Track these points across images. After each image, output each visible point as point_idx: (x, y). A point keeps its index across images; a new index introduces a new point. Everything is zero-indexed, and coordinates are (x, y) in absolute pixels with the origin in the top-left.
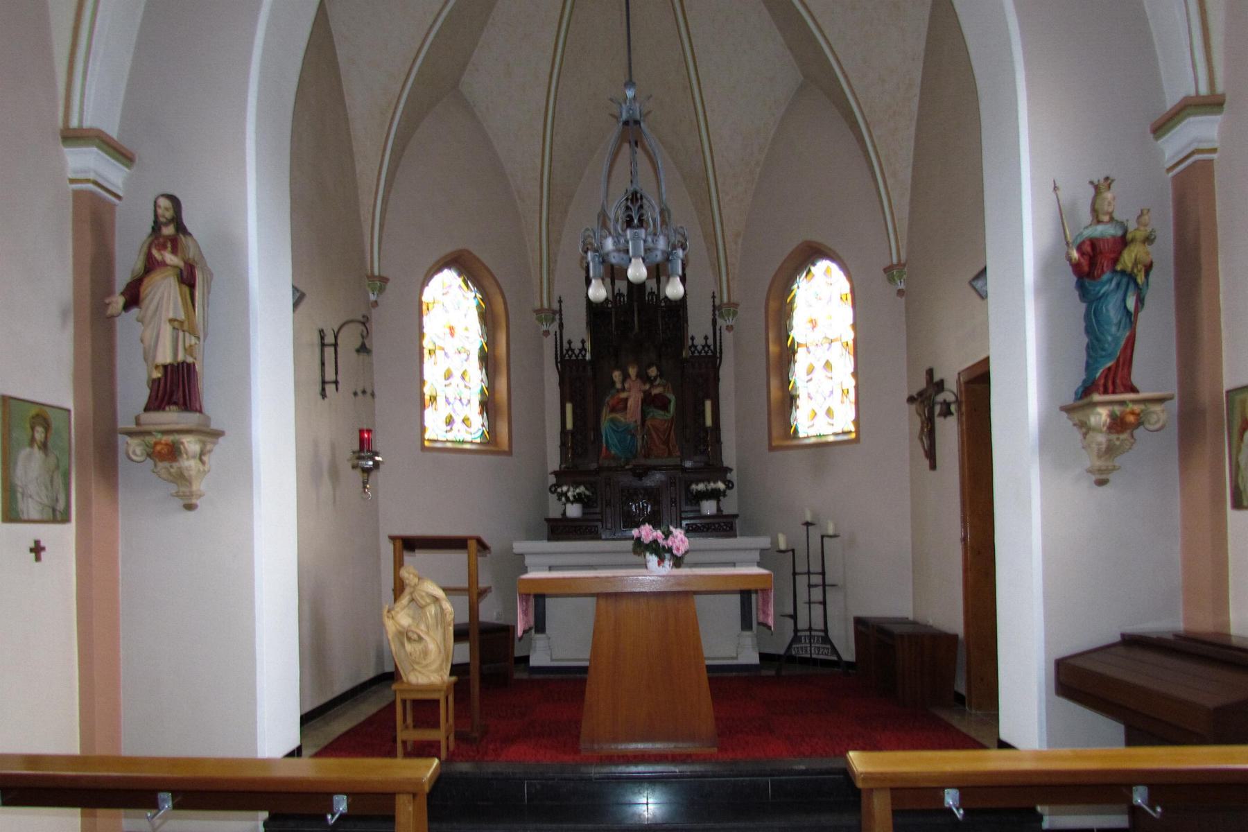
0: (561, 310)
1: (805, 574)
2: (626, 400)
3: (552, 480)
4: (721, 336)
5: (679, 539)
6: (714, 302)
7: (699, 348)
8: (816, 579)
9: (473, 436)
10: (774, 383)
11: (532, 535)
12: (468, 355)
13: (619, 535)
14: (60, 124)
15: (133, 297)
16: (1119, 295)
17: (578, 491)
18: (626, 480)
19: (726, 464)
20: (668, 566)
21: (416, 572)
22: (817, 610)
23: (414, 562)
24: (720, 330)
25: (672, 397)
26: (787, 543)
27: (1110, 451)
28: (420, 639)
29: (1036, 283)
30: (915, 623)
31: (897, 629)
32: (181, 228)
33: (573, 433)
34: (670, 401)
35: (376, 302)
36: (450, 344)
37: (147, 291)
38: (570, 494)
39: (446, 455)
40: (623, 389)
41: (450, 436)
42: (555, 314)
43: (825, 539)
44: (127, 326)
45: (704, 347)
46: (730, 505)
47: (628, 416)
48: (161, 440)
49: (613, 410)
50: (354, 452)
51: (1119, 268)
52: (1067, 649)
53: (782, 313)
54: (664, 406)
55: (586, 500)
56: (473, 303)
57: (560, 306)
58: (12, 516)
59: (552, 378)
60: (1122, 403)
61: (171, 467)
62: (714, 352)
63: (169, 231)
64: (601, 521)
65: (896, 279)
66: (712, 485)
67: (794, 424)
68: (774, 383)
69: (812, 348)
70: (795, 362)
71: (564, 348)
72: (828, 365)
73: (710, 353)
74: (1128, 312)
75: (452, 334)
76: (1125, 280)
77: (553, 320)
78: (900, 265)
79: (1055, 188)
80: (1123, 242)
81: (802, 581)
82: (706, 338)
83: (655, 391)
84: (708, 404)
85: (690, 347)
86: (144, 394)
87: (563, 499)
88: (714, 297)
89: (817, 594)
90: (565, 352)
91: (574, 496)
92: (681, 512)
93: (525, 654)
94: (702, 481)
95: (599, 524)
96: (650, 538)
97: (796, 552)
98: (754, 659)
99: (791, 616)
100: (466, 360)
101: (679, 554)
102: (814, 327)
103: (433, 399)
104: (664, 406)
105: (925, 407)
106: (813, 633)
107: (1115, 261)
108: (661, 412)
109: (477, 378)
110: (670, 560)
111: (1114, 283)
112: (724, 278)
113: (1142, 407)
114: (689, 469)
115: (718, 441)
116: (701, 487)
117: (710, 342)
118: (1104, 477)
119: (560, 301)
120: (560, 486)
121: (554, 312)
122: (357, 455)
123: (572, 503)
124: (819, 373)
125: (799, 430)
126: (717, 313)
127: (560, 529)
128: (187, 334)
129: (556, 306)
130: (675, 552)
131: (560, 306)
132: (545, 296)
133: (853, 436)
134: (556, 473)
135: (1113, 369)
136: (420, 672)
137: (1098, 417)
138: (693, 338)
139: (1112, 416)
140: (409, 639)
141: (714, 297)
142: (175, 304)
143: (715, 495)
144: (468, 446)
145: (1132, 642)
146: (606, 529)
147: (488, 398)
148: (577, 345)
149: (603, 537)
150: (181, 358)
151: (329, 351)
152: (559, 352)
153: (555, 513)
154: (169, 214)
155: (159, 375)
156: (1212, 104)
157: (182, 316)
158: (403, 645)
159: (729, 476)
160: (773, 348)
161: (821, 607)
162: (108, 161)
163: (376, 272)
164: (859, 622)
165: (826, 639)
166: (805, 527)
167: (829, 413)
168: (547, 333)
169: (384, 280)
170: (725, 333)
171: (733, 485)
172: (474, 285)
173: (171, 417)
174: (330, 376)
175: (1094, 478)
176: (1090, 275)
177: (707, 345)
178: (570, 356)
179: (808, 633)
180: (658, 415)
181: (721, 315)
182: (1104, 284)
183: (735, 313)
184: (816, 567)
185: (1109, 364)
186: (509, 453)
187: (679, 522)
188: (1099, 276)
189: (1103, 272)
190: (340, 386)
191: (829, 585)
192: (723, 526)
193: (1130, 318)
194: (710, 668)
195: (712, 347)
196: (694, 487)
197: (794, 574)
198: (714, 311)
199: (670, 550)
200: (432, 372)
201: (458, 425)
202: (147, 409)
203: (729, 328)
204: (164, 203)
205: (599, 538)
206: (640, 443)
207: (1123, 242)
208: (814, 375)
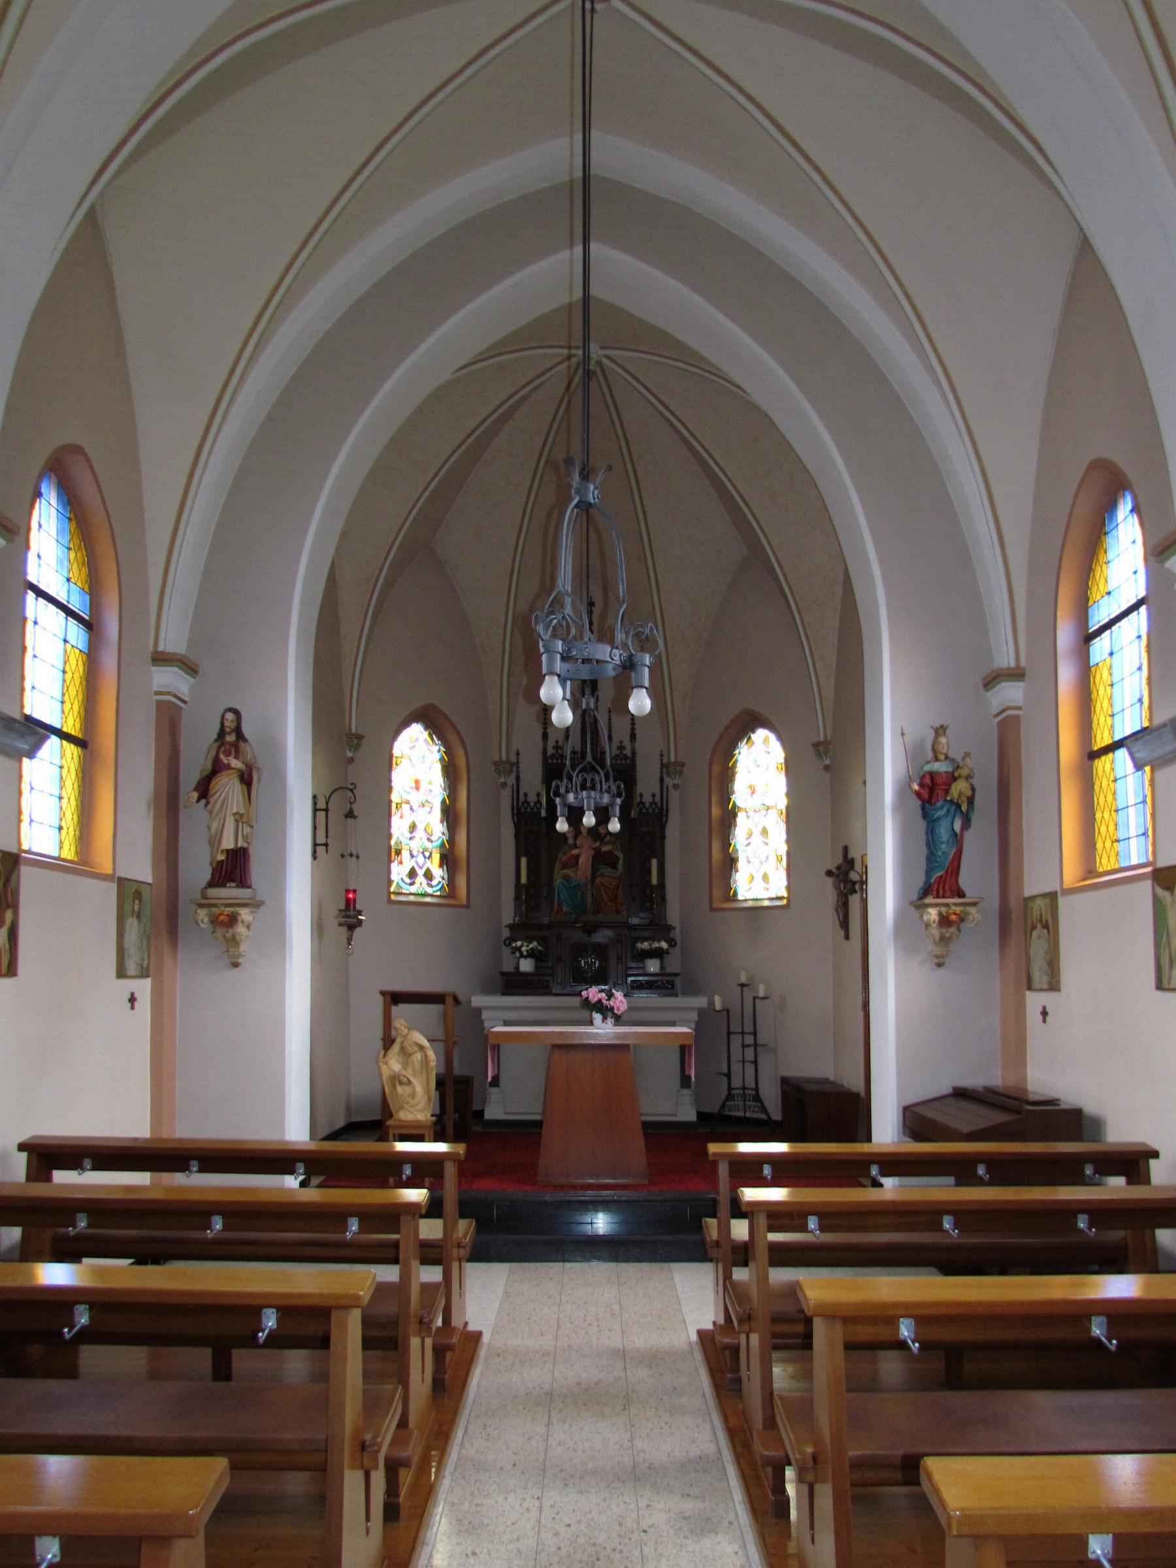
0: (518, 763)
1: (739, 1033)
2: (578, 856)
3: (506, 933)
4: (667, 794)
5: (619, 999)
6: (662, 760)
7: (647, 805)
8: (749, 1040)
9: (435, 889)
10: (716, 846)
11: (488, 990)
12: (431, 808)
13: (568, 990)
14: (151, 649)
15: (204, 789)
16: (949, 819)
17: (531, 946)
18: (576, 936)
19: (669, 923)
20: (609, 1023)
21: (406, 1025)
22: (750, 1070)
23: (401, 1012)
24: (667, 788)
25: (621, 855)
26: (723, 1003)
27: (944, 940)
28: (409, 1082)
29: (893, 803)
30: (833, 1083)
31: (809, 1087)
32: (240, 736)
33: (527, 887)
34: (618, 859)
35: (352, 758)
36: (415, 798)
37: (214, 791)
38: (524, 949)
39: (409, 908)
40: (575, 846)
41: (413, 889)
42: (511, 767)
43: (758, 1001)
44: (193, 813)
45: (651, 804)
46: (674, 964)
47: (580, 873)
48: (224, 911)
49: (565, 866)
50: (340, 911)
51: (948, 798)
52: (911, 1099)
53: (726, 777)
54: (613, 865)
55: (539, 955)
56: (437, 756)
57: (518, 759)
58: (121, 973)
59: (507, 831)
60: (947, 905)
61: (227, 932)
62: (661, 810)
63: (231, 738)
64: (552, 975)
65: (822, 755)
66: (656, 945)
67: (733, 886)
68: (716, 846)
69: (751, 813)
70: (735, 826)
71: (520, 800)
72: (765, 832)
73: (657, 811)
74: (955, 834)
75: (417, 788)
76: (953, 808)
77: (511, 772)
78: (826, 743)
79: (903, 734)
80: (953, 778)
81: (736, 1041)
82: (654, 796)
83: (606, 848)
84: (654, 862)
85: (638, 804)
86: (206, 875)
87: (518, 954)
88: (662, 755)
89: (750, 1054)
90: (520, 804)
91: (527, 951)
92: (628, 968)
93: (480, 1108)
94: (645, 939)
95: (550, 978)
96: (596, 999)
97: (731, 1012)
98: (692, 1117)
99: (725, 1075)
100: (429, 813)
101: (619, 1013)
102: (753, 793)
103: (398, 852)
104: (613, 865)
105: (840, 882)
106: (747, 1091)
107: (947, 792)
108: (610, 870)
109: (439, 830)
110: (612, 1018)
111: (945, 810)
112: (672, 739)
113: (962, 908)
114: (635, 925)
115: (663, 899)
116: (645, 945)
117: (658, 799)
118: (942, 960)
119: (518, 754)
120: (515, 941)
121: (512, 765)
122: (343, 914)
123: (526, 957)
124: (757, 839)
125: (739, 892)
126: (664, 770)
127: (513, 984)
128: (245, 825)
129: (513, 758)
130: (616, 1011)
131: (518, 759)
132: (504, 749)
133: (784, 902)
134: (510, 927)
135: (944, 877)
136: (410, 1111)
137: (929, 916)
138: (641, 795)
139: (940, 914)
140: (401, 1083)
141: (662, 755)
142: (238, 800)
143: (658, 954)
144: (428, 899)
145: (960, 1094)
146: (557, 983)
147: (448, 850)
148: (532, 798)
149: (554, 991)
150: (239, 845)
151: (321, 815)
152: (515, 805)
153: (508, 967)
154: (233, 725)
155: (223, 858)
156: (1017, 674)
157: (242, 812)
158: (394, 1086)
159: (672, 935)
160: (716, 811)
161: (753, 1066)
162: (185, 678)
163: (354, 731)
164: (785, 1081)
165: (757, 1098)
166: (740, 988)
167: (765, 878)
168: (504, 785)
169: (360, 737)
170: (671, 790)
171: (676, 943)
172: (439, 739)
173: (230, 892)
174: (321, 839)
175: (936, 961)
176: (929, 801)
177: (653, 802)
178: (526, 809)
179: (741, 1092)
180: (609, 871)
181: (669, 775)
182: (937, 810)
183: (681, 772)
184: (749, 1028)
185: (939, 874)
186: (467, 906)
187: (624, 979)
188: (935, 803)
189: (938, 800)
190: (329, 848)
191: (761, 1045)
192: (664, 985)
193: (957, 840)
194: (645, 1125)
195: (659, 805)
196: (639, 945)
197: (729, 1033)
198: (662, 769)
199: (612, 1009)
200: (399, 828)
201: (420, 878)
202: (211, 884)
203: (676, 787)
204: (230, 716)
205: (549, 993)
206: (589, 901)
207: (953, 778)
208: (752, 840)
